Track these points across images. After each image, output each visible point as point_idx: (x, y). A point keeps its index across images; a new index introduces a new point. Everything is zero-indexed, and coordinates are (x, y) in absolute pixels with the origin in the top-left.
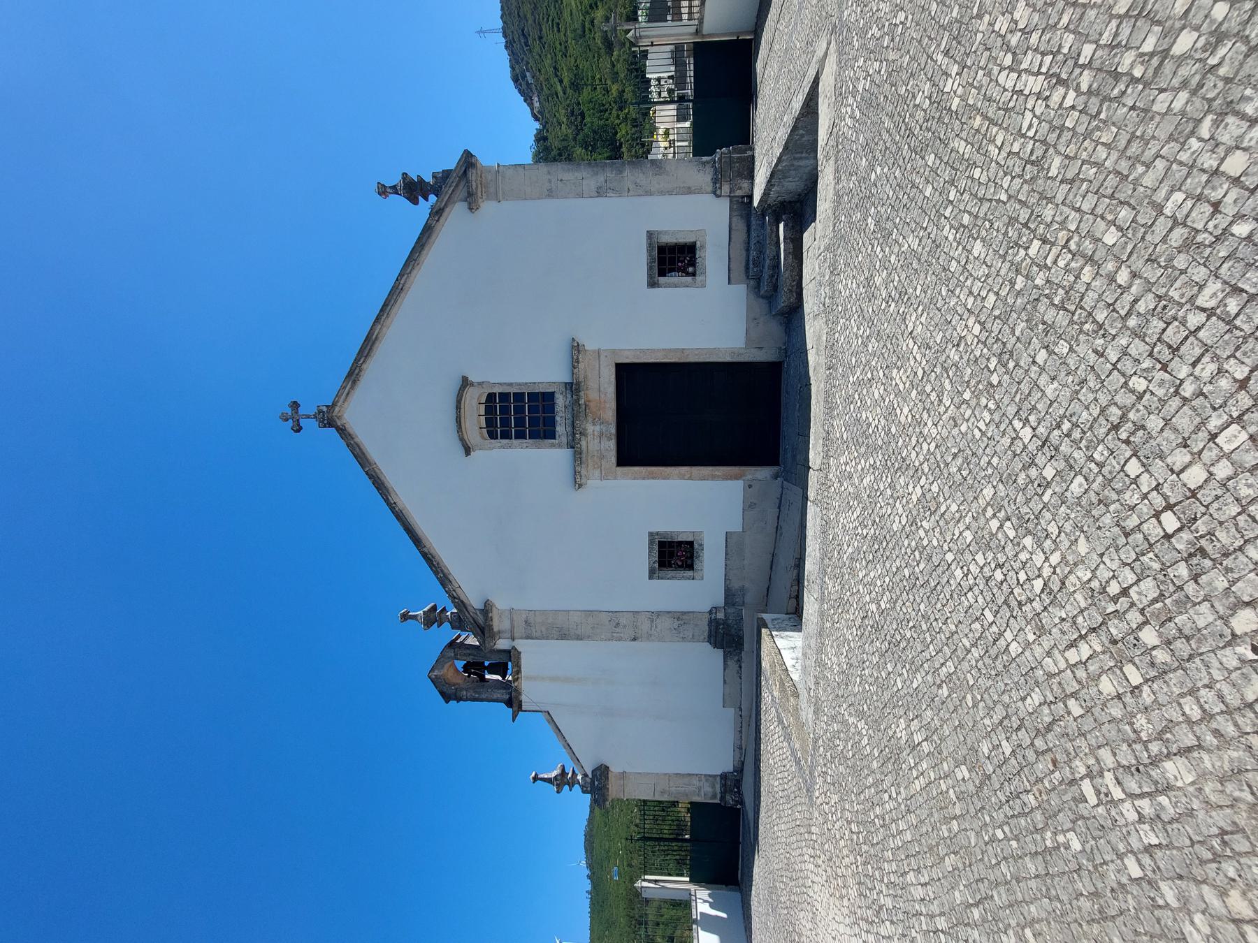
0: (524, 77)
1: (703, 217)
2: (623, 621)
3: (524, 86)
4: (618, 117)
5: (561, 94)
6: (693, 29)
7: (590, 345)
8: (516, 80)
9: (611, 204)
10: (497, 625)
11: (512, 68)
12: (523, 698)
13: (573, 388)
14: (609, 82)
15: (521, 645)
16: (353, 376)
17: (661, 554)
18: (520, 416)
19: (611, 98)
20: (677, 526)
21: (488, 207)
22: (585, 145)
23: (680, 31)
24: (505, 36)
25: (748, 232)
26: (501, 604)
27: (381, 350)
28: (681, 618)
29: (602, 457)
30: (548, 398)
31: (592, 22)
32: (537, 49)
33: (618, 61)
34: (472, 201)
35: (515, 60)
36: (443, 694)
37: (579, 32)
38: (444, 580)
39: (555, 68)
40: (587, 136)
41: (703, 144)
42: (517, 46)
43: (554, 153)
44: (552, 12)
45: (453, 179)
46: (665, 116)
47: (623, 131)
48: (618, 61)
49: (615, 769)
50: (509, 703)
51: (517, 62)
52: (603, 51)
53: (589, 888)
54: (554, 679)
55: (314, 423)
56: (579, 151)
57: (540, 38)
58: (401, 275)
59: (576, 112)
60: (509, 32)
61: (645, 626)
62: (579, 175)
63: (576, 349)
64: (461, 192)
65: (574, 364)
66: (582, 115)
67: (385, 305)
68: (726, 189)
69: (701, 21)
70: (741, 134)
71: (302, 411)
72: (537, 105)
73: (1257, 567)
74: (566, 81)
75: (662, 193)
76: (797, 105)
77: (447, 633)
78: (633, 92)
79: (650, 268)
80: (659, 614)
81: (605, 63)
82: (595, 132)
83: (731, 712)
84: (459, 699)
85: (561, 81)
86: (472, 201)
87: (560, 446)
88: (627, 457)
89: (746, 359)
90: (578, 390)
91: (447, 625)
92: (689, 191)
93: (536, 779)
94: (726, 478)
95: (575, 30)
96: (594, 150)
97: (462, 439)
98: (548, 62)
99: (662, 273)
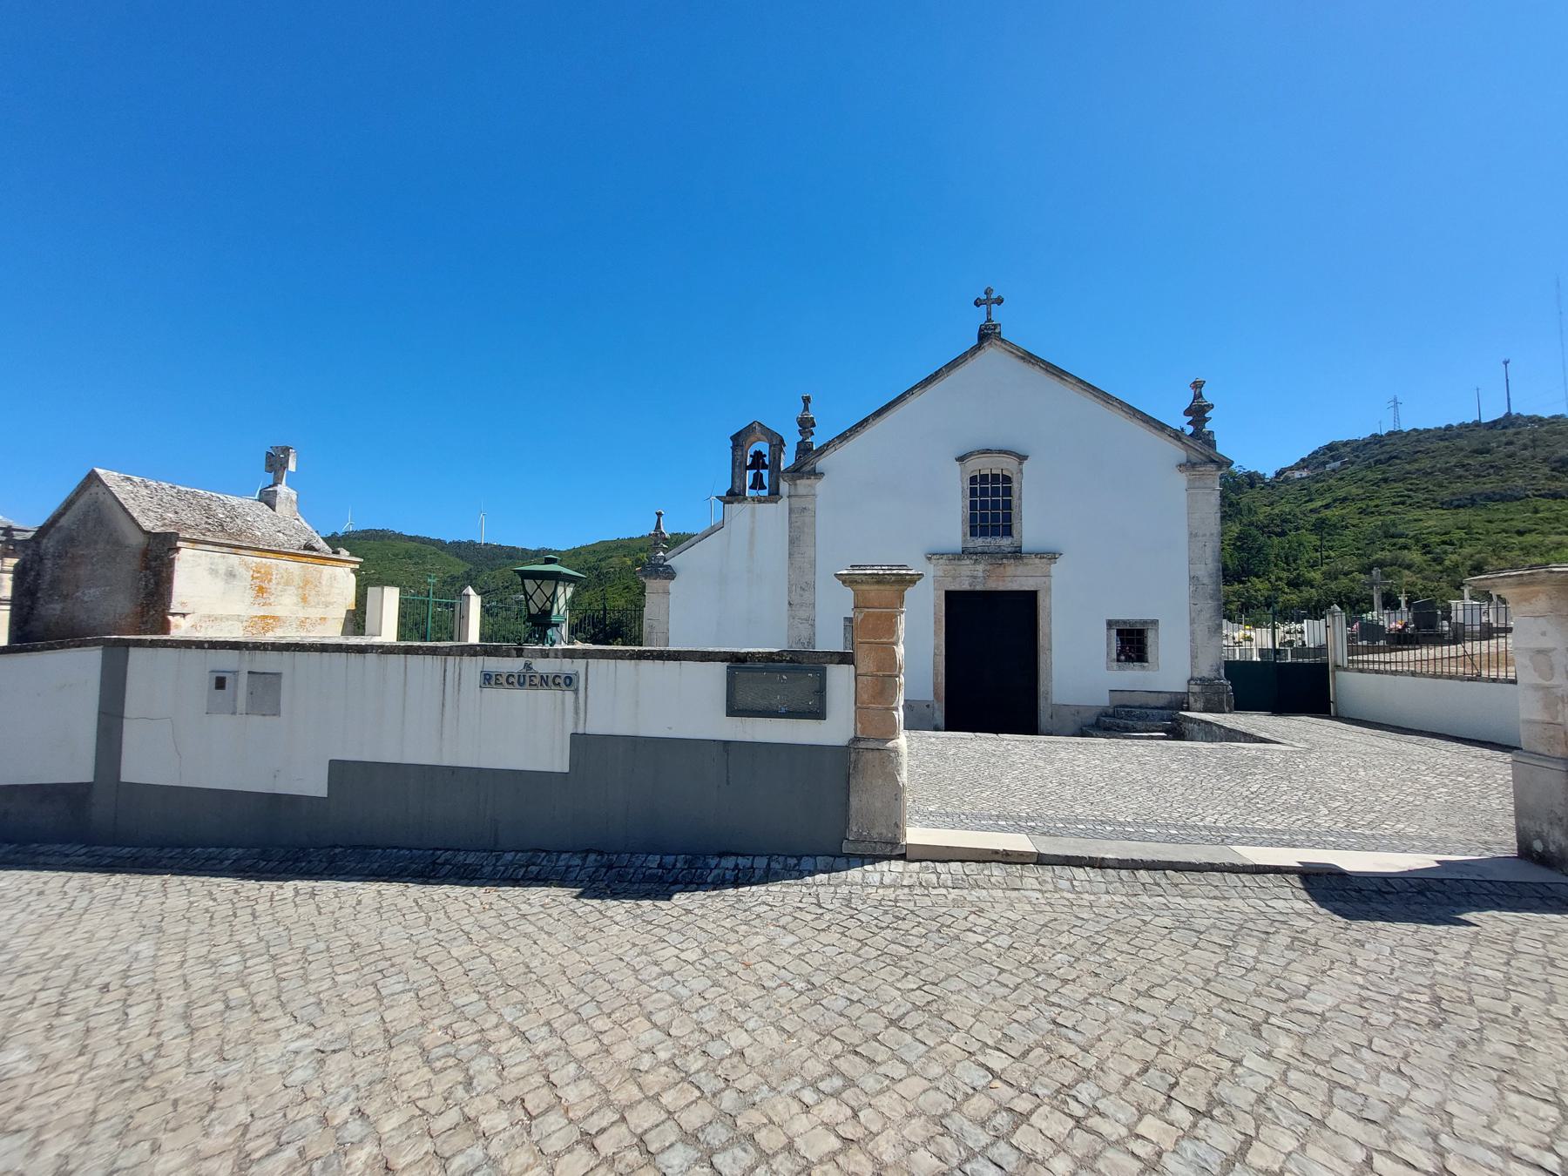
0: (1334, 459)
1: (1171, 667)
2: (806, 594)
3: (1322, 459)
4: (1279, 579)
5: (1311, 506)
6: (1339, 662)
7: (1055, 568)
8: (1331, 447)
9: (1182, 591)
10: (803, 485)
11: (1346, 444)
12: (736, 505)
13: (1017, 553)
14: (1325, 568)
15: (783, 504)
16: (1029, 358)
18: (991, 505)
19: (1303, 570)
21: (1182, 479)
23: (1338, 653)
24: (1390, 434)
25: (1162, 708)
26: (820, 486)
27: (1054, 382)
29: (954, 578)
30: (1008, 531)
31: (1405, 547)
32: (1371, 476)
33: (1353, 580)
34: (1188, 466)
35: (1357, 447)
36: (738, 434)
37: (1392, 530)
38: (843, 437)
39: (1345, 499)
40: (1255, 540)
41: (1235, 670)
42: (1376, 449)
43: (1233, 496)
44: (1421, 496)
45: (1208, 451)
46: (1262, 638)
47: (1260, 587)
48: (1353, 580)
49: (672, 585)
51: (1354, 450)
54: (752, 532)
55: (983, 320)
56: (1236, 529)
58: (1121, 402)
59: (1287, 527)
60: (1394, 439)
61: (803, 613)
62: (1209, 561)
63: (1052, 556)
64: (1195, 457)
65: (1040, 555)
66: (1283, 534)
67: (1094, 388)
68: (1196, 689)
69: (1346, 670)
70: (1243, 704)
71: (994, 306)
72: (1297, 475)
73: (825, 1173)
74: (1328, 513)
75: (1192, 633)
76: (1263, 735)
77: (792, 438)
78: (1310, 599)
79: (1125, 622)
80: (813, 625)
81: (1350, 563)
82: (1260, 550)
83: (315, 784)
84: (734, 448)
85: (1327, 506)
86: (1188, 466)
87: (964, 541)
89: (1042, 703)
90: (1016, 558)
92: (1194, 657)
93: (659, 514)
95: (1394, 525)
97: (971, 454)
98: (1354, 490)
99: (1119, 632)
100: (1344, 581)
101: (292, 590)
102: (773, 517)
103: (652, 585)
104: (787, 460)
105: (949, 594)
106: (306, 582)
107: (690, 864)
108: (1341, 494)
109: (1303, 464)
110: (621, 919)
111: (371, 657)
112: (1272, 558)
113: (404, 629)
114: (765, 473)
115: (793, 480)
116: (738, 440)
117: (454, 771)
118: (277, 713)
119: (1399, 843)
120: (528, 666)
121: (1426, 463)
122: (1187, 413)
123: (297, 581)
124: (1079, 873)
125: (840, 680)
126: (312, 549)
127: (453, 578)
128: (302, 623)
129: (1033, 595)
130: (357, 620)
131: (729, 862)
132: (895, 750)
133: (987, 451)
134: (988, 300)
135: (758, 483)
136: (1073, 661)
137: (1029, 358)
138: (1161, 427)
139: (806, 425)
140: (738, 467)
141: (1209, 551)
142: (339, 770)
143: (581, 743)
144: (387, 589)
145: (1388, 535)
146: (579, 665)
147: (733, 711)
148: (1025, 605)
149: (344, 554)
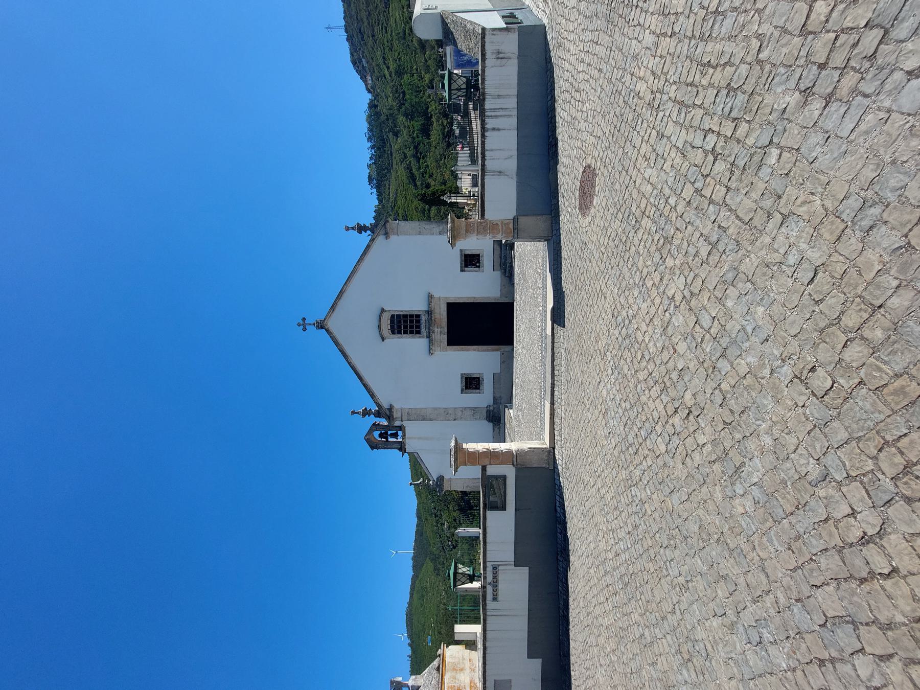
0: (361, 62)
3: (361, 68)
5: (388, 76)
7: (436, 295)
8: (354, 63)
10: (396, 414)
11: (352, 55)
12: (406, 447)
13: (429, 313)
15: (405, 424)
16: (333, 307)
17: (466, 383)
18: (405, 324)
20: (473, 371)
21: (393, 238)
22: (406, 115)
24: (346, 31)
26: (397, 406)
27: (345, 295)
28: (474, 410)
30: (418, 316)
34: (387, 235)
35: (354, 50)
38: (372, 395)
39: (384, 58)
42: (355, 40)
44: (382, 18)
49: (446, 477)
50: (400, 450)
51: (356, 51)
52: (418, 51)
53: (410, 653)
54: (420, 438)
57: (373, 36)
59: (400, 90)
63: (430, 297)
64: (383, 232)
65: (429, 304)
66: (404, 93)
72: (370, 82)
74: (391, 67)
77: (372, 419)
80: (465, 409)
81: (420, 59)
83: (537, 663)
84: (377, 448)
85: (388, 68)
86: (387, 235)
88: (451, 342)
91: (372, 416)
94: (493, 350)
95: (399, 34)
96: (412, 119)
97: (381, 335)
98: (379, 53)
99: (466, 266)
100: (430, 62)
101: (458, 676)
102: (412, 428)
103: (446, 487)
104: (384, 422)
105: (449, 344)
106: (454, 669)
107: (560, 523)
108: (381, 60)
109: (364, 78)
110: (575, 559)
111: (487, 645)
112: (417, 100)
113: (476, 621)
114: (389, 432)
115: (393, 419)
116: (374, 446)
117: (529, 610)
118: (510, 681)
119: (544, 287)
120: (489, 584)
121: (364, 14)
122: (361, 233)
123: (454, 674)
124: (556, 393)
125: (492, 470)
126: (439, 667)
127: (435, 570)
128: (472, 670)
129: (450, 305)
130: (470, 644)
131: (558, 509)
132: (517, 451)
133: (379, 326)
134: (304, 324)
135: (395, 435)
136: (480, 287)
137: (333, 307)
138: (368, 247)
139: (366, 413)
140: (387, 446)
141: (427, 227)
142: (530, 656)
143: (517, 564)
144: (456, 631)
145: (405, 38)
146: (488, 564)
147: (504, 508)
148: (453, 308)
149: (440, 652)
